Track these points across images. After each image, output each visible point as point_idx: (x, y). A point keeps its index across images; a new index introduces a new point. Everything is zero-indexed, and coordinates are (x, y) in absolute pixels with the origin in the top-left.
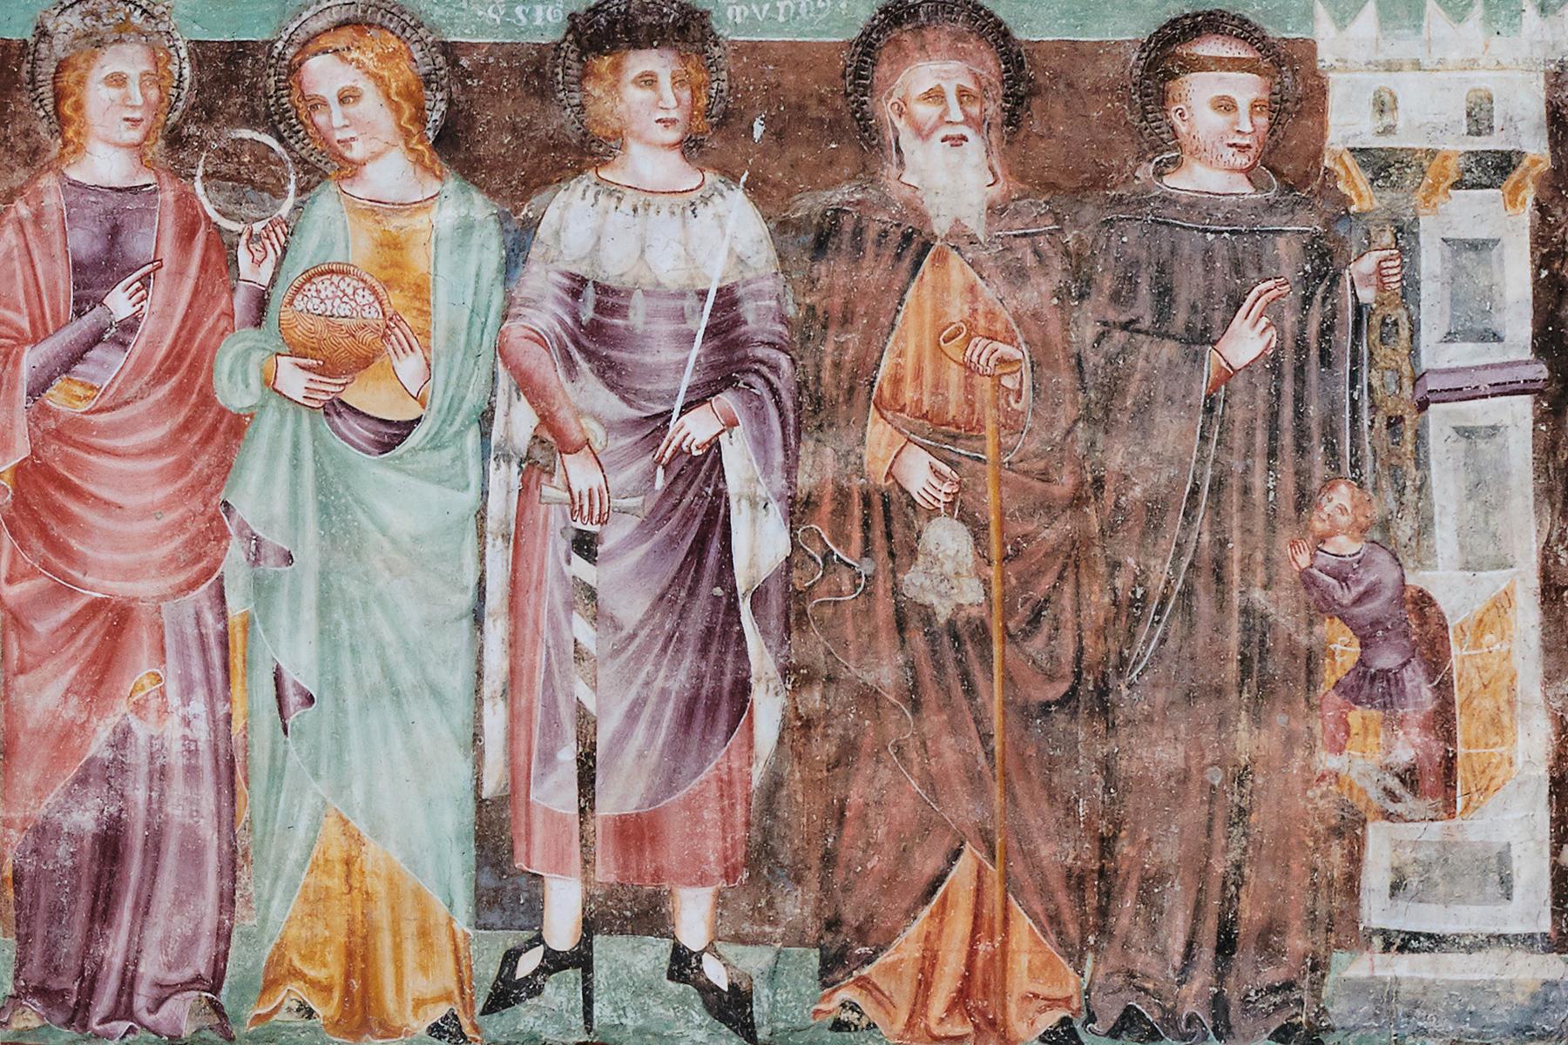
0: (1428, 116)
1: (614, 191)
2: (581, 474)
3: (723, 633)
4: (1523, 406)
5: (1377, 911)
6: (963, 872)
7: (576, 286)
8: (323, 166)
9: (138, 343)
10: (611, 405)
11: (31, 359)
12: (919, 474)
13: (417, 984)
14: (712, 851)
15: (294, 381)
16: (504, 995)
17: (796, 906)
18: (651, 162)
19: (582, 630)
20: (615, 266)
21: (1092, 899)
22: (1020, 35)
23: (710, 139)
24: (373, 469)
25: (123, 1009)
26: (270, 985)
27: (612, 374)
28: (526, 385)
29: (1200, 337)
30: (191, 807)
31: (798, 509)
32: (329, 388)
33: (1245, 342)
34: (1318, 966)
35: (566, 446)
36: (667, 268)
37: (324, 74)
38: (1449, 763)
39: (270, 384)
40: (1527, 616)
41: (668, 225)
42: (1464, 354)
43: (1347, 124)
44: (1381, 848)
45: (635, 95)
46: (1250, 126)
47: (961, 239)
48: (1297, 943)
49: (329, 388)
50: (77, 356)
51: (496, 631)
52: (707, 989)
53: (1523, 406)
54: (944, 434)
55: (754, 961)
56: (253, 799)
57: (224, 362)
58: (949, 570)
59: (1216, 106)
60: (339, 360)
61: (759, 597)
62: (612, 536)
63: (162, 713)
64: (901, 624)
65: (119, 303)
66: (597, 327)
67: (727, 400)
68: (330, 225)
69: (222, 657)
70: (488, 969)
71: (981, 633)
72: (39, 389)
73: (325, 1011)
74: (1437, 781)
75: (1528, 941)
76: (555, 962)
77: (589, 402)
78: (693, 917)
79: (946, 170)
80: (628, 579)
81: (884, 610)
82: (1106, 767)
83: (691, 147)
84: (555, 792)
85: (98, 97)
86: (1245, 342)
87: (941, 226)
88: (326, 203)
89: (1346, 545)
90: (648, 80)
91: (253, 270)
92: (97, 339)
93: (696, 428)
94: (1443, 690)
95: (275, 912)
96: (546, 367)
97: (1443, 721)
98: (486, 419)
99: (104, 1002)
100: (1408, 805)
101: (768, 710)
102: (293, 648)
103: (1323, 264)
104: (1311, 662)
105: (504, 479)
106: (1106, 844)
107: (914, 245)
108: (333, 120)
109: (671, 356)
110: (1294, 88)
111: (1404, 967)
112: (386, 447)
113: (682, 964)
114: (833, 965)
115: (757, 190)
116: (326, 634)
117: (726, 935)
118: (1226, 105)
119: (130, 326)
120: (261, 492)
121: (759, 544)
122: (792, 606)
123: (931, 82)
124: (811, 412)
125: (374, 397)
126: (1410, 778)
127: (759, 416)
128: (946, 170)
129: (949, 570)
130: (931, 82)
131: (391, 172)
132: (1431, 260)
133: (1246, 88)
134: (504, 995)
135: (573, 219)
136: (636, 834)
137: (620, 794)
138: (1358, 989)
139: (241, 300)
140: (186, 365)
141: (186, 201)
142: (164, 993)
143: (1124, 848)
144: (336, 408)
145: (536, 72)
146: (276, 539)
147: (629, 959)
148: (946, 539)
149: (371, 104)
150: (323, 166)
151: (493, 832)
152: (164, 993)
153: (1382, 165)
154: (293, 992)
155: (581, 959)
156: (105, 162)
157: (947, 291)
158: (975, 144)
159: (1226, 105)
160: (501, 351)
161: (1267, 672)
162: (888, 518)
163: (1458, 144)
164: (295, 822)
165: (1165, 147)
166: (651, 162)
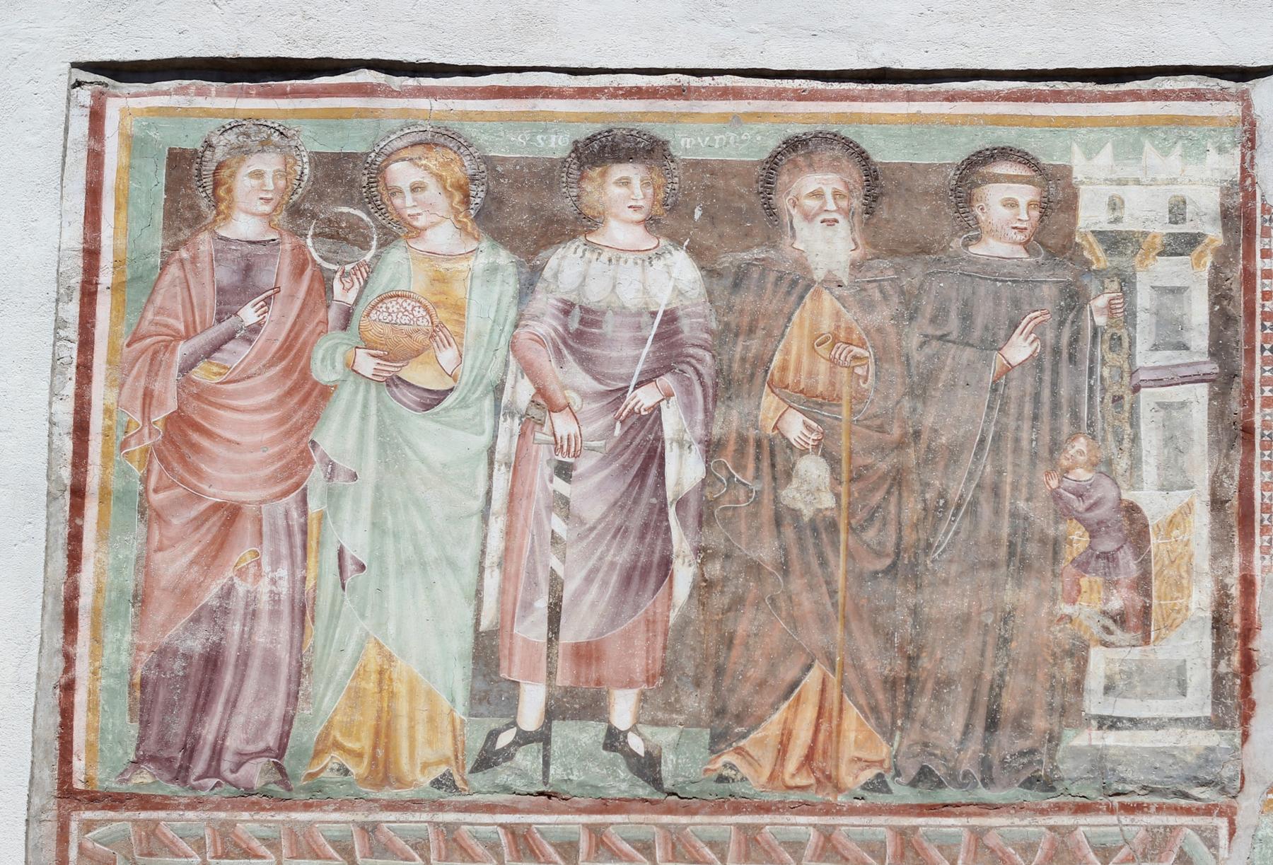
0: (1144, 212)
1: (595, 247)
2: (563, 425)
3: (656, 525)
4: (1202, 390)
5: (1095, 704)
6: (812, 680)
7: (567, 309)
8: (396, 231)
9: (260, 340)
10: (586, 382)
11: (183, 349)
12: (796, 427)
13: (424, 753)
14: (638, 666)
15: (366, 364)
16: (487, 761)
17: (694, 702)
18: (622, 232)
19: (558, 524)
20: (595, 294)
21: (901, 693)
22: (876, 158)
23: (665, 220)
24: (419, 426)
25: (213, 769)
26: (318, 754)
27: (586, 362)
28: (528, 369)
29: (991, 345)
30: (272, 636)
31: (711, 448)
32: (390, 369)
33: (1019, 350)
34: (1053, 739)
35: (553, 408)
36: (630, 297)
37: (402, 174)
38: (1146, 611)
39: (351, 367)
40: (1202, 519)
41: (633, 269)
42: (1163, 358)
43: (1091, 215)
44: (1099, 662)
45: (615, 191)
46: (1027, 217)
47: (832, 282)
48: (1040, 723)
49: (390, 369)
50: (217, 347)
51: (497, 526)
52: (630, 755)
53: (1202, 390)
54: (812, 402)
55: (665, 737)
56: (316, 633)
57: (318, 354)
58: (812, 487)
59: (1006, 204)
60: (394, 353)
61: (681, 504)
62: (583, 465)
63: (260, 577)
64: (778, 522)
65: (249, 315)
66: (581, 331)
67: (667, 380)
68: (399, 268)
69: (302, 540)
70: (476, 743)
71: (833, 526)
72: (186, 368)
73: (358, 770)
74: (1138, 622)
75: (1195, 723)
76: (524, 739)
77: (573, 380)
78: (623, 709)
79: (823, 237)
80: (593, 492)
81: (767, 512)
82: (915, 612)
83: (651, 223)
84: (532, 629)
85: (243, 184)
86: (1019, 350)
87: (819, 275)
88: (396, 255)
89: (1082, 475)
90: (625, 182)
91: (343, 293)
92: (231, 337)
93: (645, 398)
94: (1145, 564)
95: (326, 702)
96: (545, 361)
97: (1143, 584)
98: (498, 389)
99: (199, 766)
100: (1119, 635)
101: (684, 575)
102: (352, 532)
103: (1073, 300)
104: (1055, 547)
105: (510, 426)
106: (912, 660)
107: (799, 284)
108: (406, 204)
109: (627, 353)
110: (1057, 197)
111: (1112, 739)
112: (427, 407)
113: (614, 740)
114: (719, 741)
115: (696, 252)
116: (377, 526)
117: (646, 717)
118: (1011, 204)
119: (255, 329)
120: (336, 436)
121: (684, 470)
122: (705, 512)
123: (818, 186)
124: (724, 387)
125: (420, 375)
126: (1120, 619)
127: (689, 392)
128: (823, 237)
129: (812, 487)
130: (818, 186)
131: (442, 236)
132: (1144, 298)
133: (1026, 194)
134: (487, 761)
135: (567, 266)
136: (586, 654)
137: (573, 631)
138: (1077, 753)
139: (333, 314)
140: (293, 352)
141: (300, 250)
142: (243, 759)
143: (925, 662)
144: (395, 382)
145: (544, 175)
146: (346, 464)
147: (578, 737)
148: (812, 469)
149: (433, 191)
150: (396, 231)
151: (486, 652)
152: (243, 759)
153: (1113, 242)
154: (333, 759)
155: (543, 737)
156: (244, 225)
157: (824, 310)
158: (843, 226)
159: (1011, 204)
160: (512, 346)
161: (1024, 554)
162: (774, 457)
163: (1161, 228)
164: (341, 645)
165: (972, 229)
166: (622, 232)
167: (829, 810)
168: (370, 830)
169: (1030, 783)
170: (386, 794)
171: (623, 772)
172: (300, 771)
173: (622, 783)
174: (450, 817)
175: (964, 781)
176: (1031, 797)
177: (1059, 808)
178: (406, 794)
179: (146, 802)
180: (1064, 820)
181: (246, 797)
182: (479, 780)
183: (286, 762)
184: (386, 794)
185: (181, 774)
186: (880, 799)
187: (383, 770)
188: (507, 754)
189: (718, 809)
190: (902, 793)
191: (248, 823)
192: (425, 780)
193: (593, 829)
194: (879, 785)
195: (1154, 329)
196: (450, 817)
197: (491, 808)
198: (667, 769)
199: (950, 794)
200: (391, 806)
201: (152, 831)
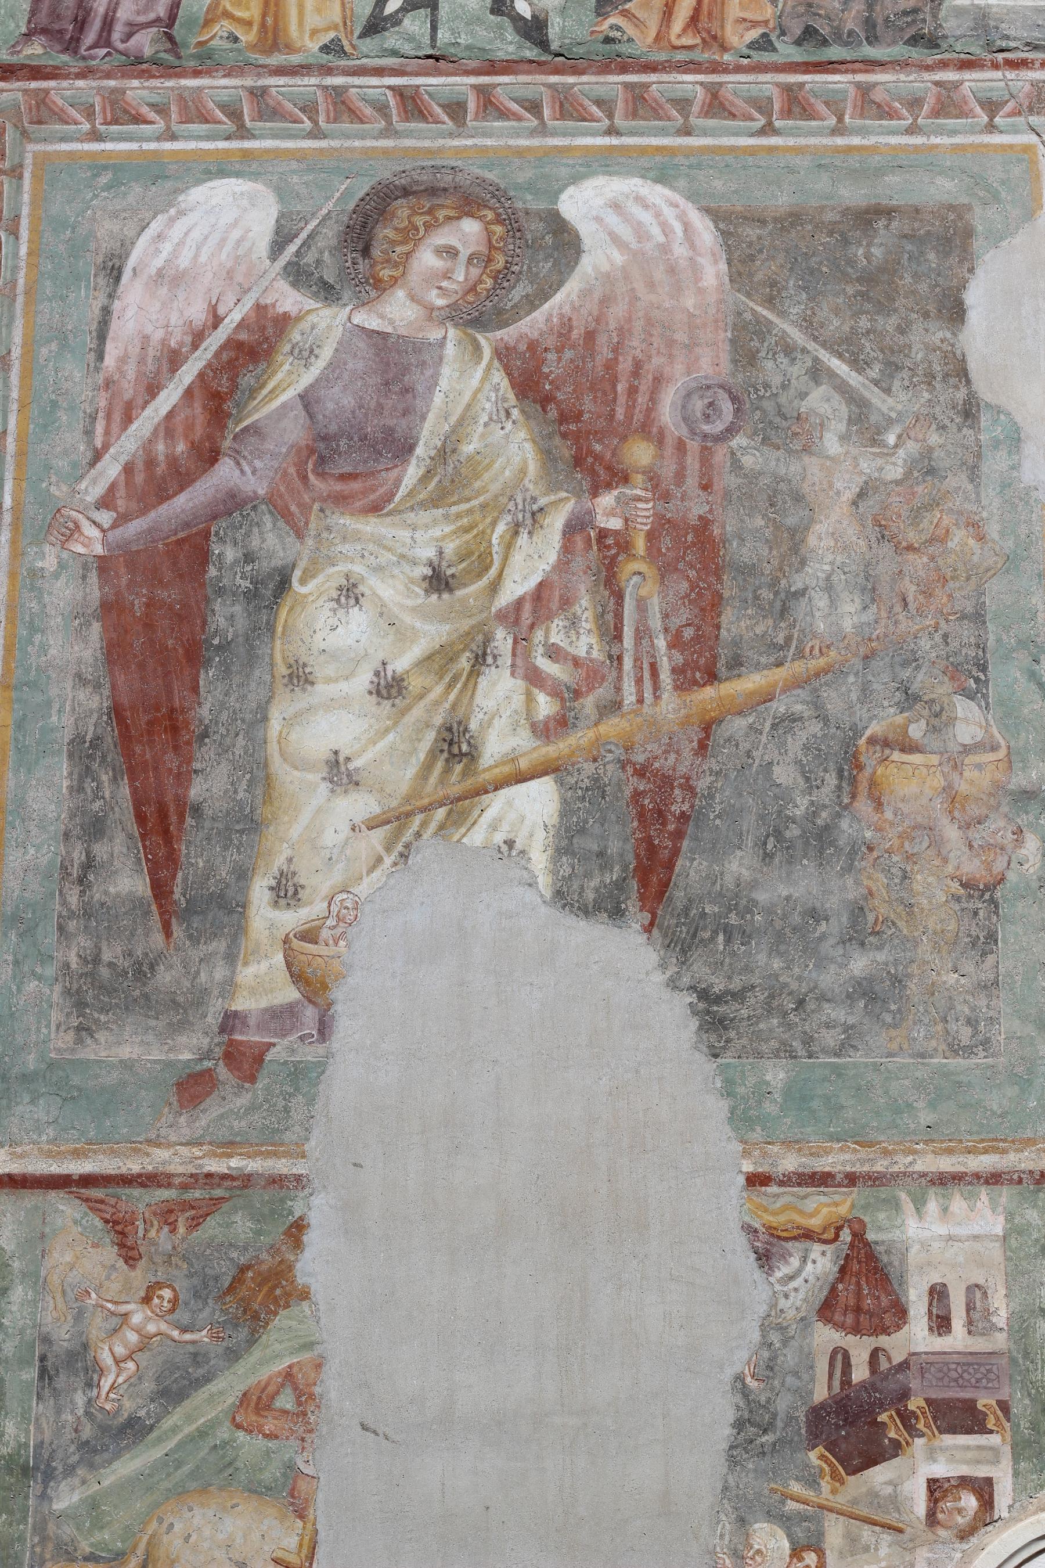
25: (104, 39)
26: (208, 23)
52: (517, 19)
73: (247, 37)
99: (90, 37)
142: (133, 29)
152: (133, 29)
154: (222, 28)
167: (716, 68)
168: (258, 94)
169: (915, 40)
170: (276, 59)
171: (510, 35)
172: (190, 40)
173: (509, 45)
174: (338, 81)
175: (848, 40)
176: (915, 54)
177: (944, 65)
178: (295, 59)
179: (36, 73)
180: (950, 76)
181: (137, 65)
182: (368, 45)
183: (177, 31)
184: (276, 59)
185: (72, 45)
186: (766, 57)
187: (272, 37)
188: (395, 20)
189: (605, 69)
190: (787, 51)
191: (137, 91)
192: (314, 46)
193: (479, 89)
194: (764, 44)
195: (226, 617)
196: (338, 81)
197: (379, 72)
198: (553, 32)
199: (835, 52)
200: (280, 71)
201: (42, 99)
